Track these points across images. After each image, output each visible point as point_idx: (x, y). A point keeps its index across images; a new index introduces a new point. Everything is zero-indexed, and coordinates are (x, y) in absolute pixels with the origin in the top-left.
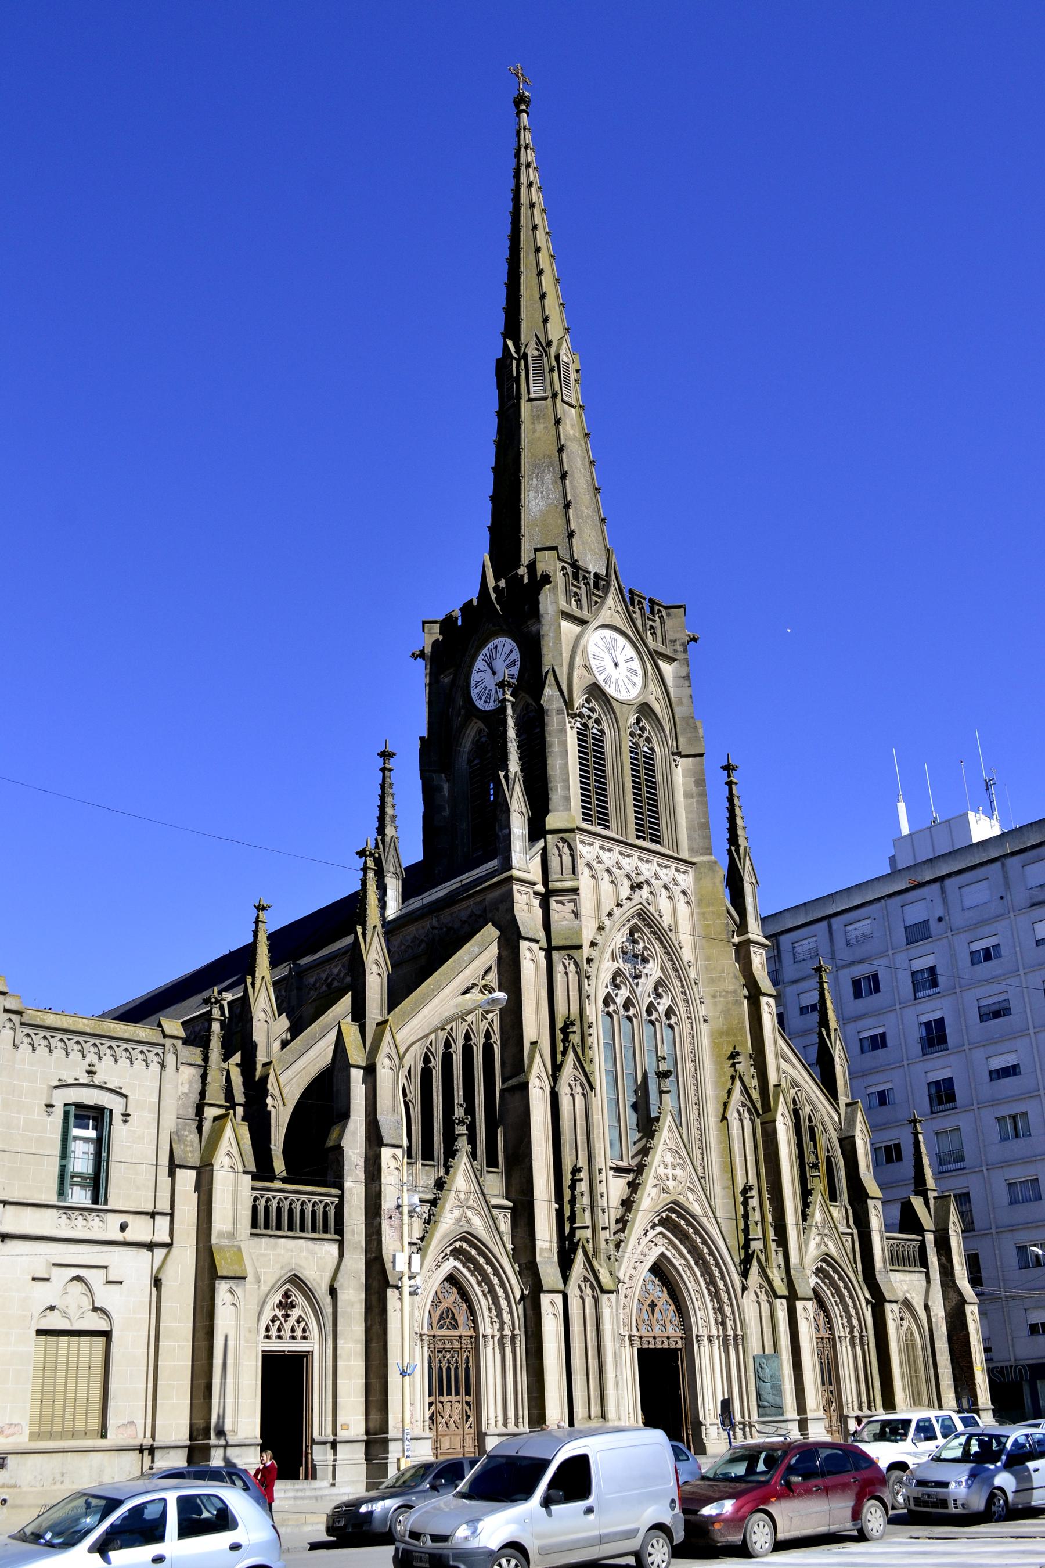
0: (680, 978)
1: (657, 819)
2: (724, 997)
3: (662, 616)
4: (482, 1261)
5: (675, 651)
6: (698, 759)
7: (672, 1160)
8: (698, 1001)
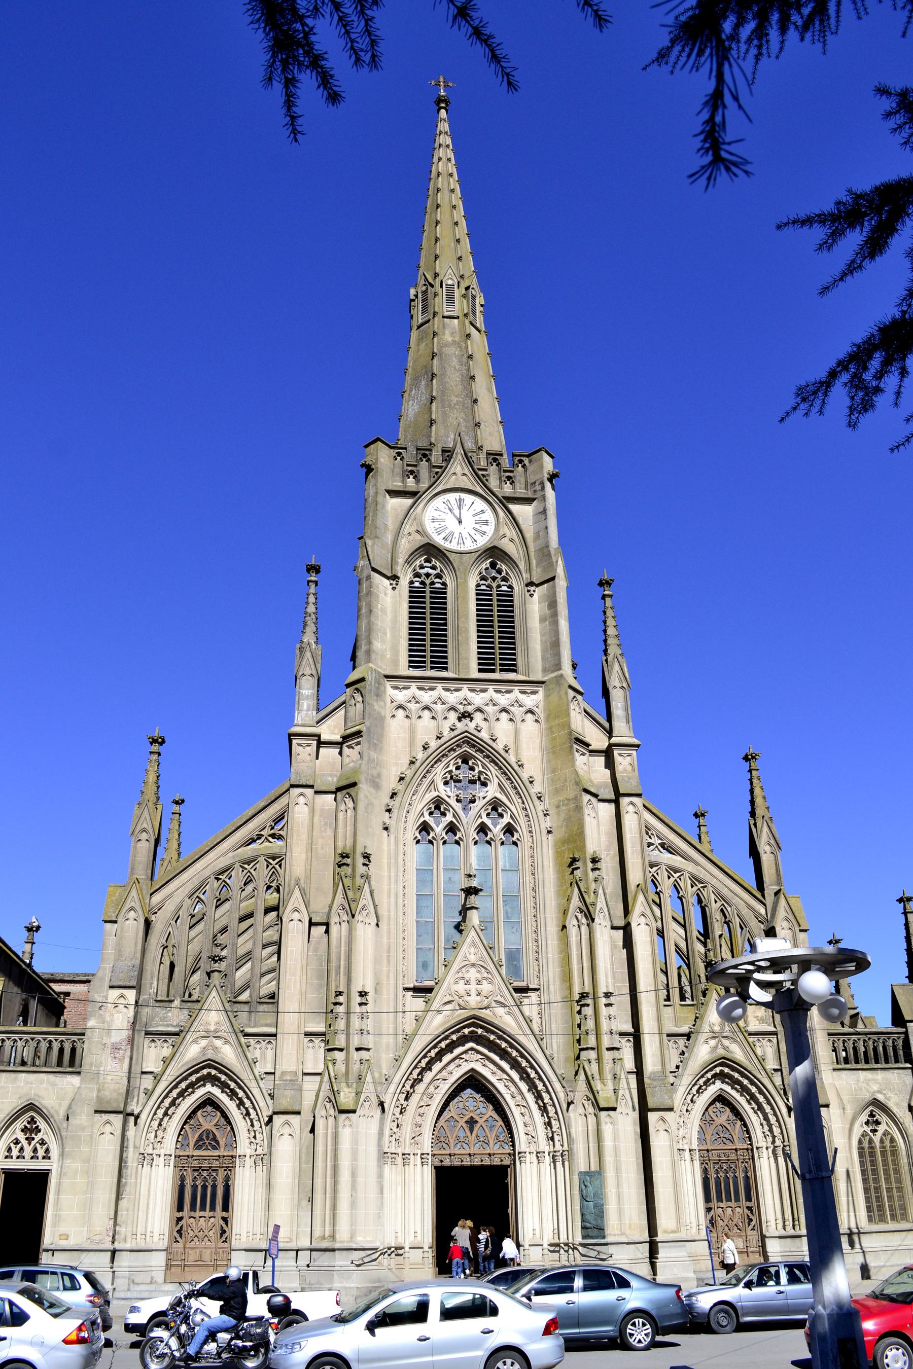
0: (520, 795)
2: (567, 805)
3: (525, 465)
4: (746, 1082)
6: (551, 583)
8: (541, 814)
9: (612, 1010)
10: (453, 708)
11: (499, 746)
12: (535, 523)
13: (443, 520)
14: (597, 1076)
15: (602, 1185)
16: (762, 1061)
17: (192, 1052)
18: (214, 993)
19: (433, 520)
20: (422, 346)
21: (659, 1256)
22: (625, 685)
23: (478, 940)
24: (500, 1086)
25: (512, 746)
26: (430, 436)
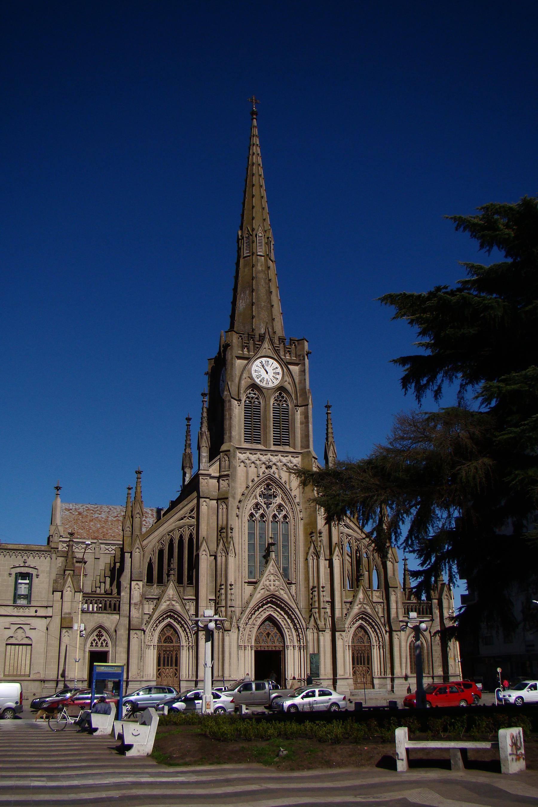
4: (371, 621)
5: (300, 360)
8: (298, 511)
9: (324, 593)
10: (264, 463)
11: (283, 481)
12: (299, 375)
13: (260, 372)
14: (318, 618)
15: (319, 658)
16: (377, 613)
17: (164, 606)
18: (172, 583)
19: (256, 371)
20: (246, 270)
21: (337, 684)
22: (335, 456)
23: (274, 564)
24: (280, 620)
25: (287, 481)
26: (252, 325)
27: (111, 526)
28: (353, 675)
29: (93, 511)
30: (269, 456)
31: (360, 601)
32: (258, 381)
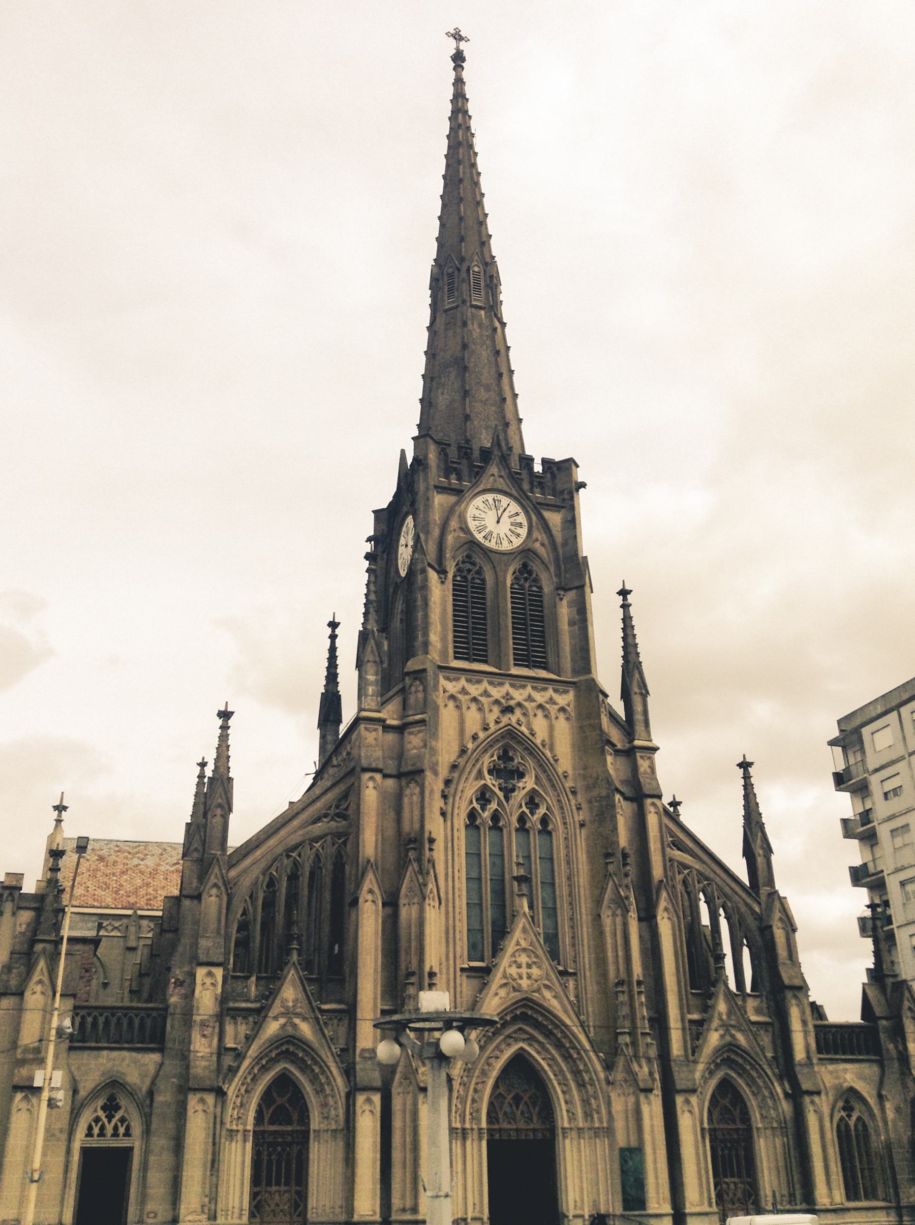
1: (485, 640)
2: (598, 801)
5: (564, 500)
7: (527, 959)
8: (574, 808)
10: (497, 702)
12: (563, 529)
13: (483, 519)
16: (762, 1049)
17: (272, 1028)
18: (292, 972)
19: (475, 518)
27: (163, 883)
28: (717, 1204)
29: (129, 853)
30: (507, 687)
31: (721, 1019)
32: (479, 537)
